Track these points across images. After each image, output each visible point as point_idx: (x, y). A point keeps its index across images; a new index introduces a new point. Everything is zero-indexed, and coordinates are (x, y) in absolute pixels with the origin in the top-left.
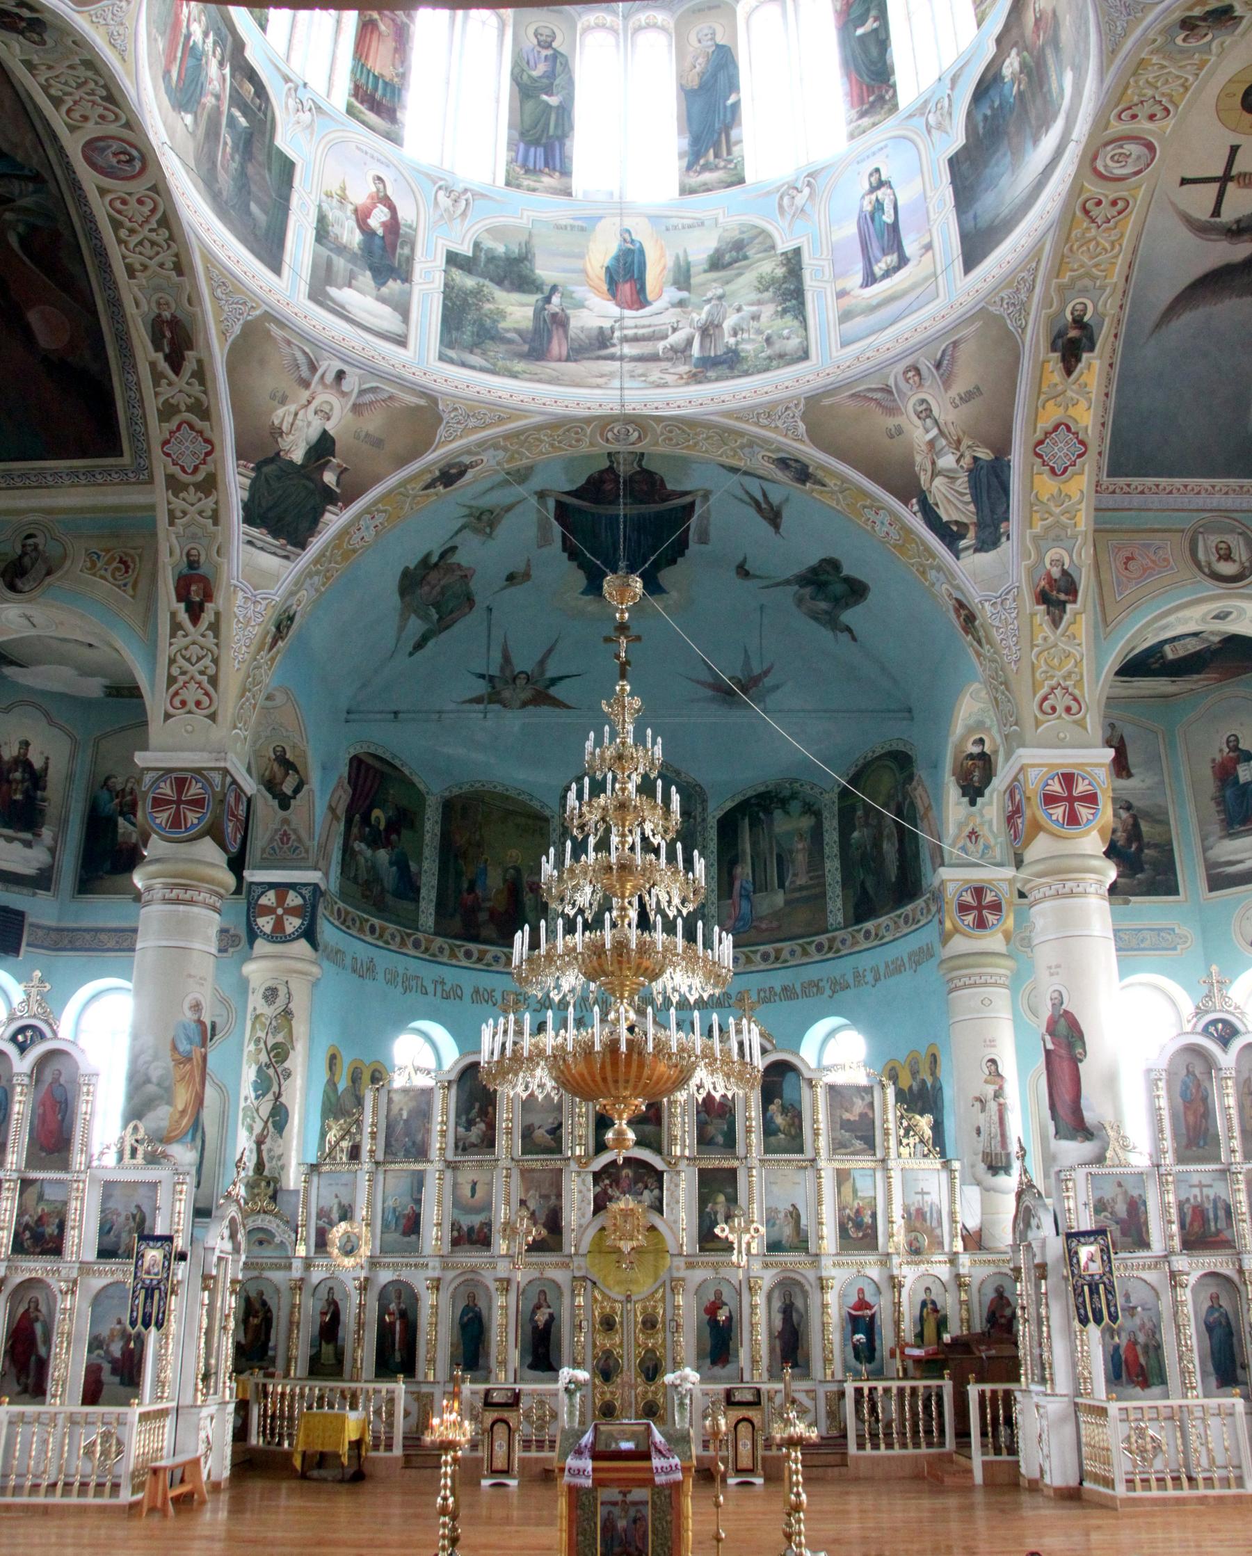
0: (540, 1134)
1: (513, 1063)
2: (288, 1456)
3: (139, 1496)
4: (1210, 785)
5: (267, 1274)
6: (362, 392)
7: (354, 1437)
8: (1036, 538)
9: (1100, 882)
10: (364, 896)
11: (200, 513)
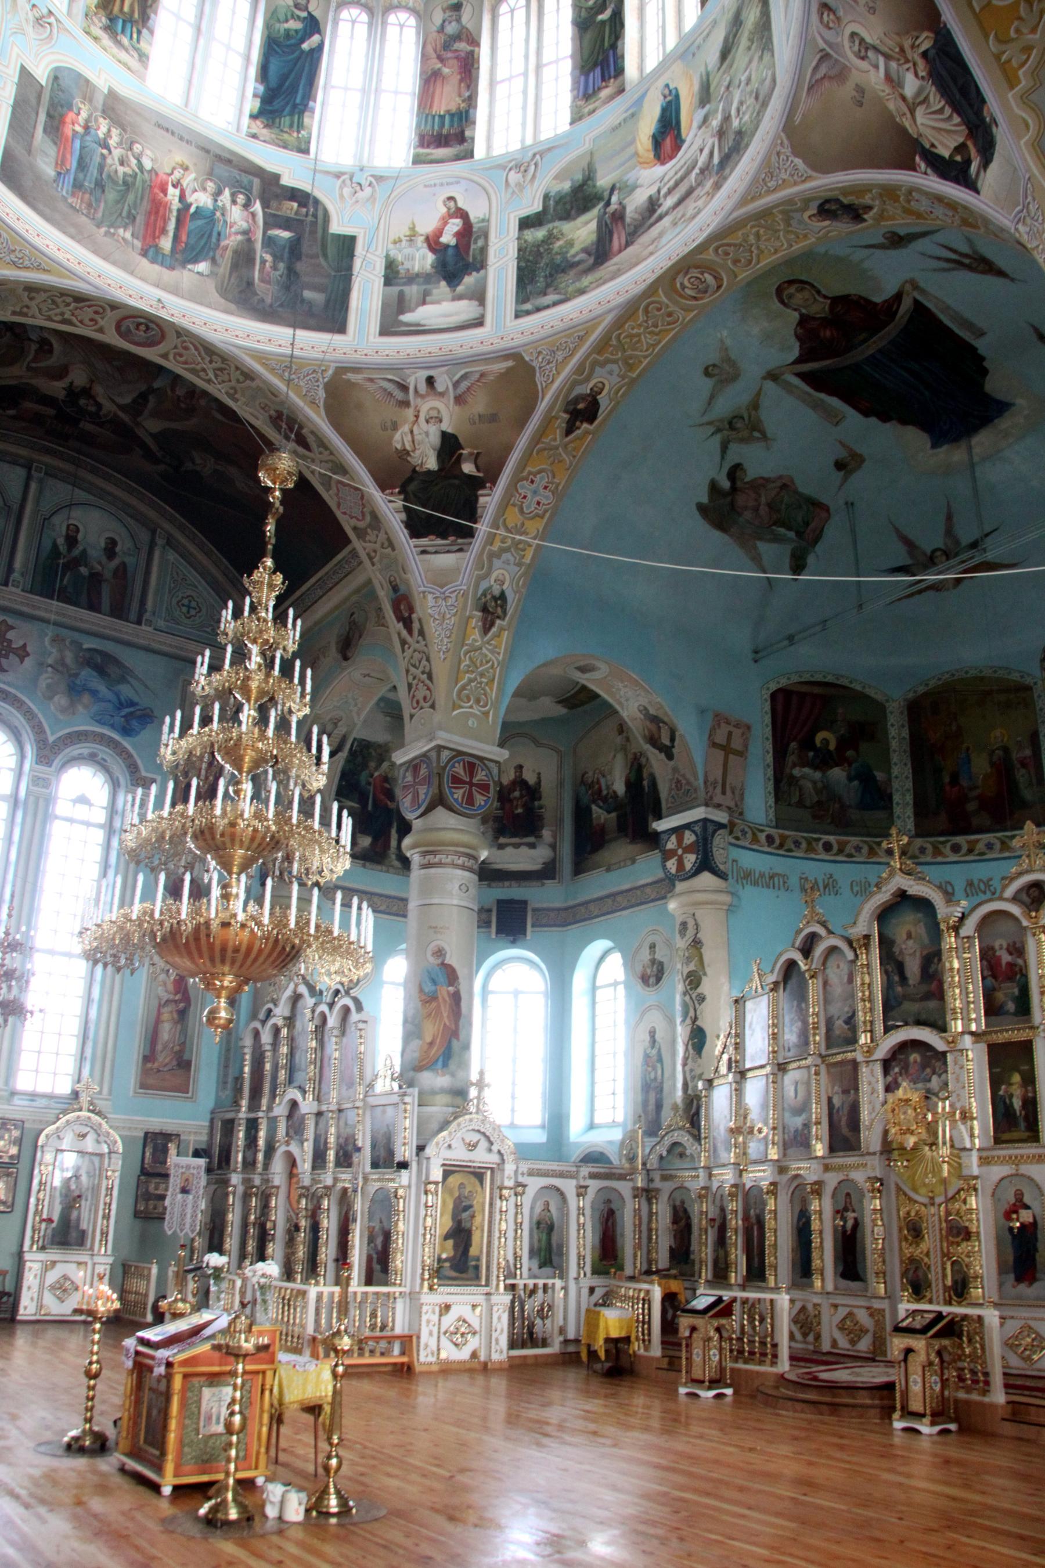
6: (456, 385)
7: (614, 1334)
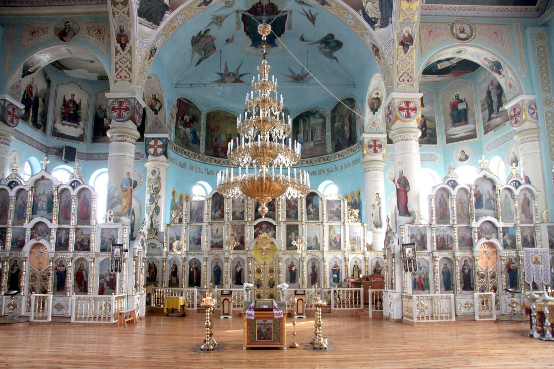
0: (238, 214)
1: (228, 185)
2: (163, 309)
3: (116, 321)
4: (449, 111)
5: (155, 257)
7: (182, 304)
8: (400, 23)
9: (416, 136)
10: (182, 143)
11: (123, 13)
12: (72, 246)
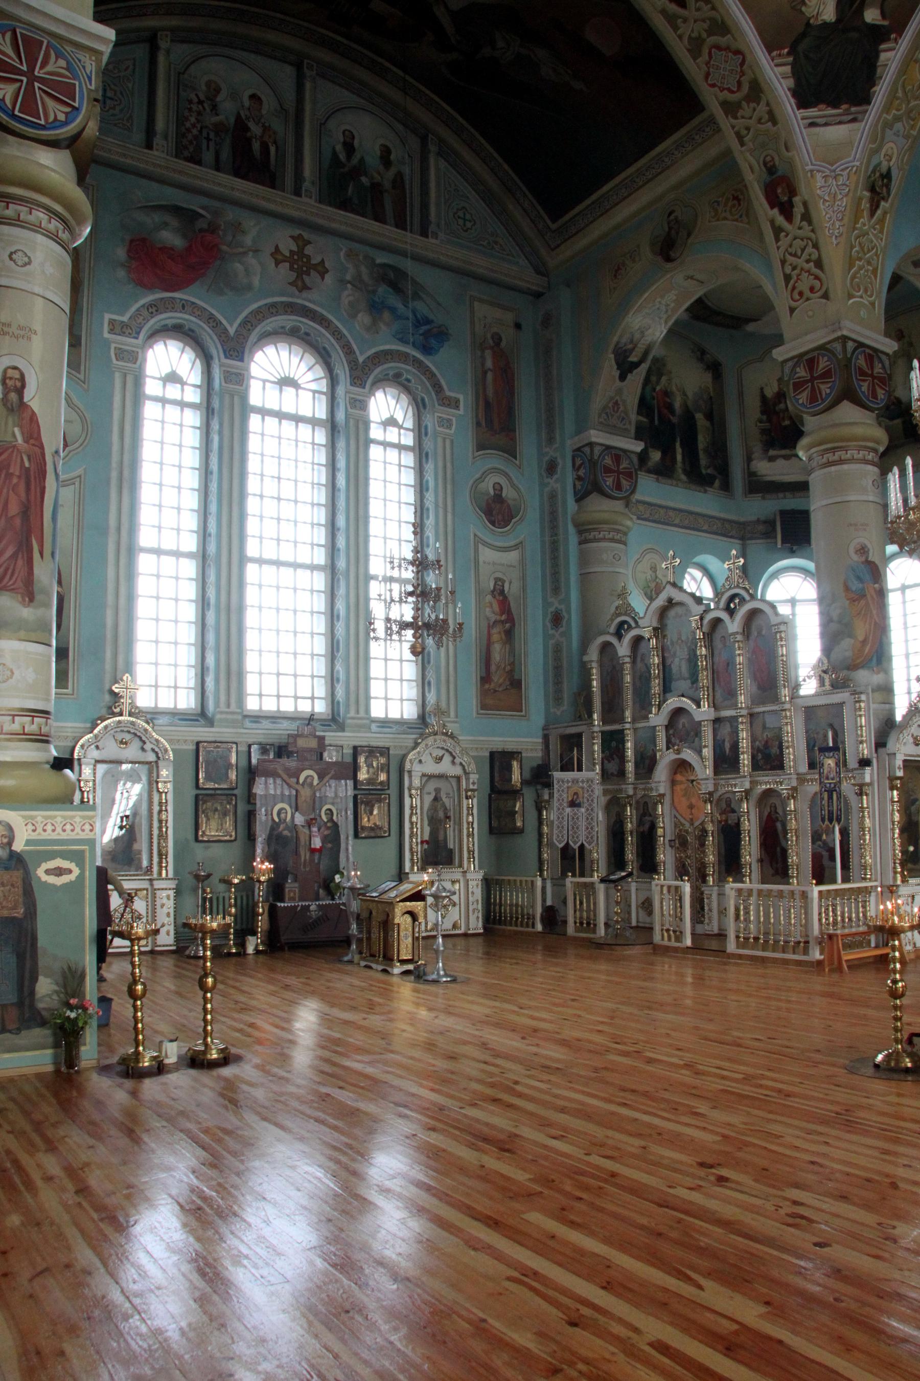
12: (745, 759)
